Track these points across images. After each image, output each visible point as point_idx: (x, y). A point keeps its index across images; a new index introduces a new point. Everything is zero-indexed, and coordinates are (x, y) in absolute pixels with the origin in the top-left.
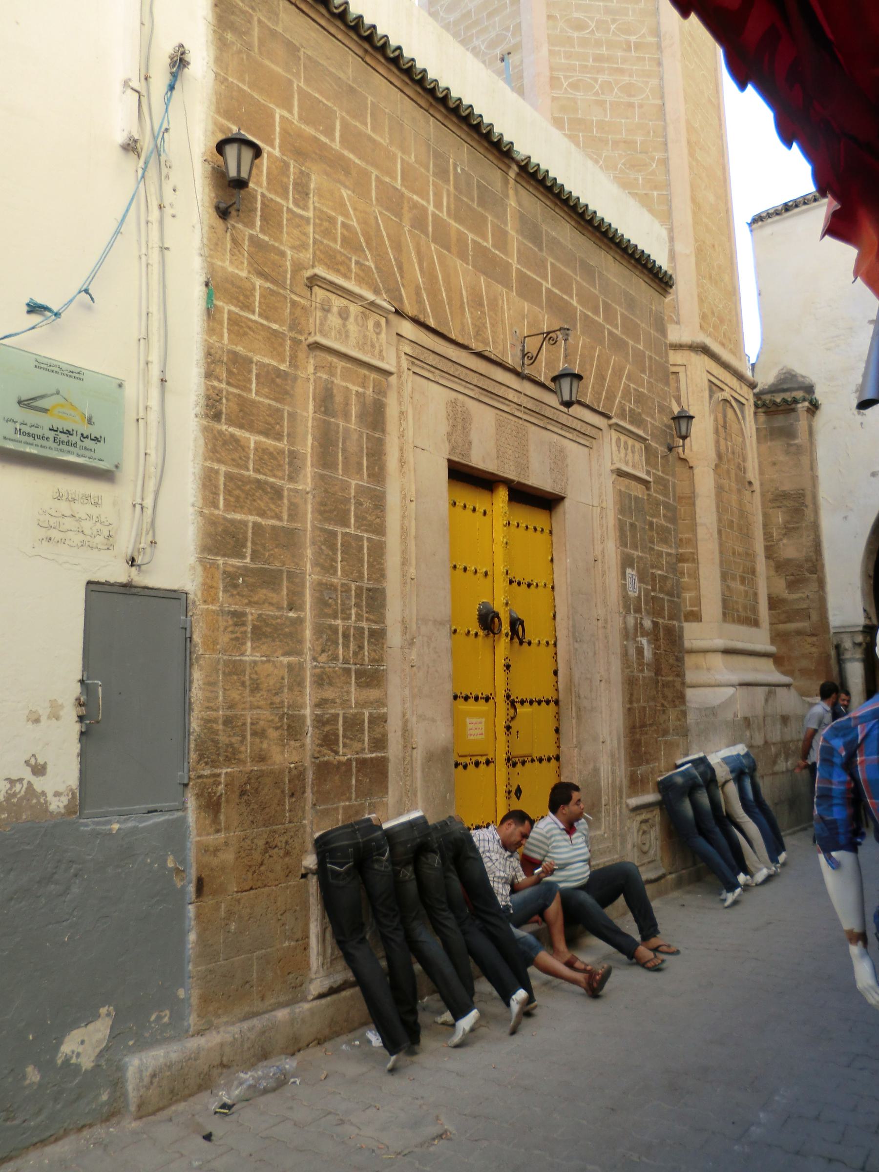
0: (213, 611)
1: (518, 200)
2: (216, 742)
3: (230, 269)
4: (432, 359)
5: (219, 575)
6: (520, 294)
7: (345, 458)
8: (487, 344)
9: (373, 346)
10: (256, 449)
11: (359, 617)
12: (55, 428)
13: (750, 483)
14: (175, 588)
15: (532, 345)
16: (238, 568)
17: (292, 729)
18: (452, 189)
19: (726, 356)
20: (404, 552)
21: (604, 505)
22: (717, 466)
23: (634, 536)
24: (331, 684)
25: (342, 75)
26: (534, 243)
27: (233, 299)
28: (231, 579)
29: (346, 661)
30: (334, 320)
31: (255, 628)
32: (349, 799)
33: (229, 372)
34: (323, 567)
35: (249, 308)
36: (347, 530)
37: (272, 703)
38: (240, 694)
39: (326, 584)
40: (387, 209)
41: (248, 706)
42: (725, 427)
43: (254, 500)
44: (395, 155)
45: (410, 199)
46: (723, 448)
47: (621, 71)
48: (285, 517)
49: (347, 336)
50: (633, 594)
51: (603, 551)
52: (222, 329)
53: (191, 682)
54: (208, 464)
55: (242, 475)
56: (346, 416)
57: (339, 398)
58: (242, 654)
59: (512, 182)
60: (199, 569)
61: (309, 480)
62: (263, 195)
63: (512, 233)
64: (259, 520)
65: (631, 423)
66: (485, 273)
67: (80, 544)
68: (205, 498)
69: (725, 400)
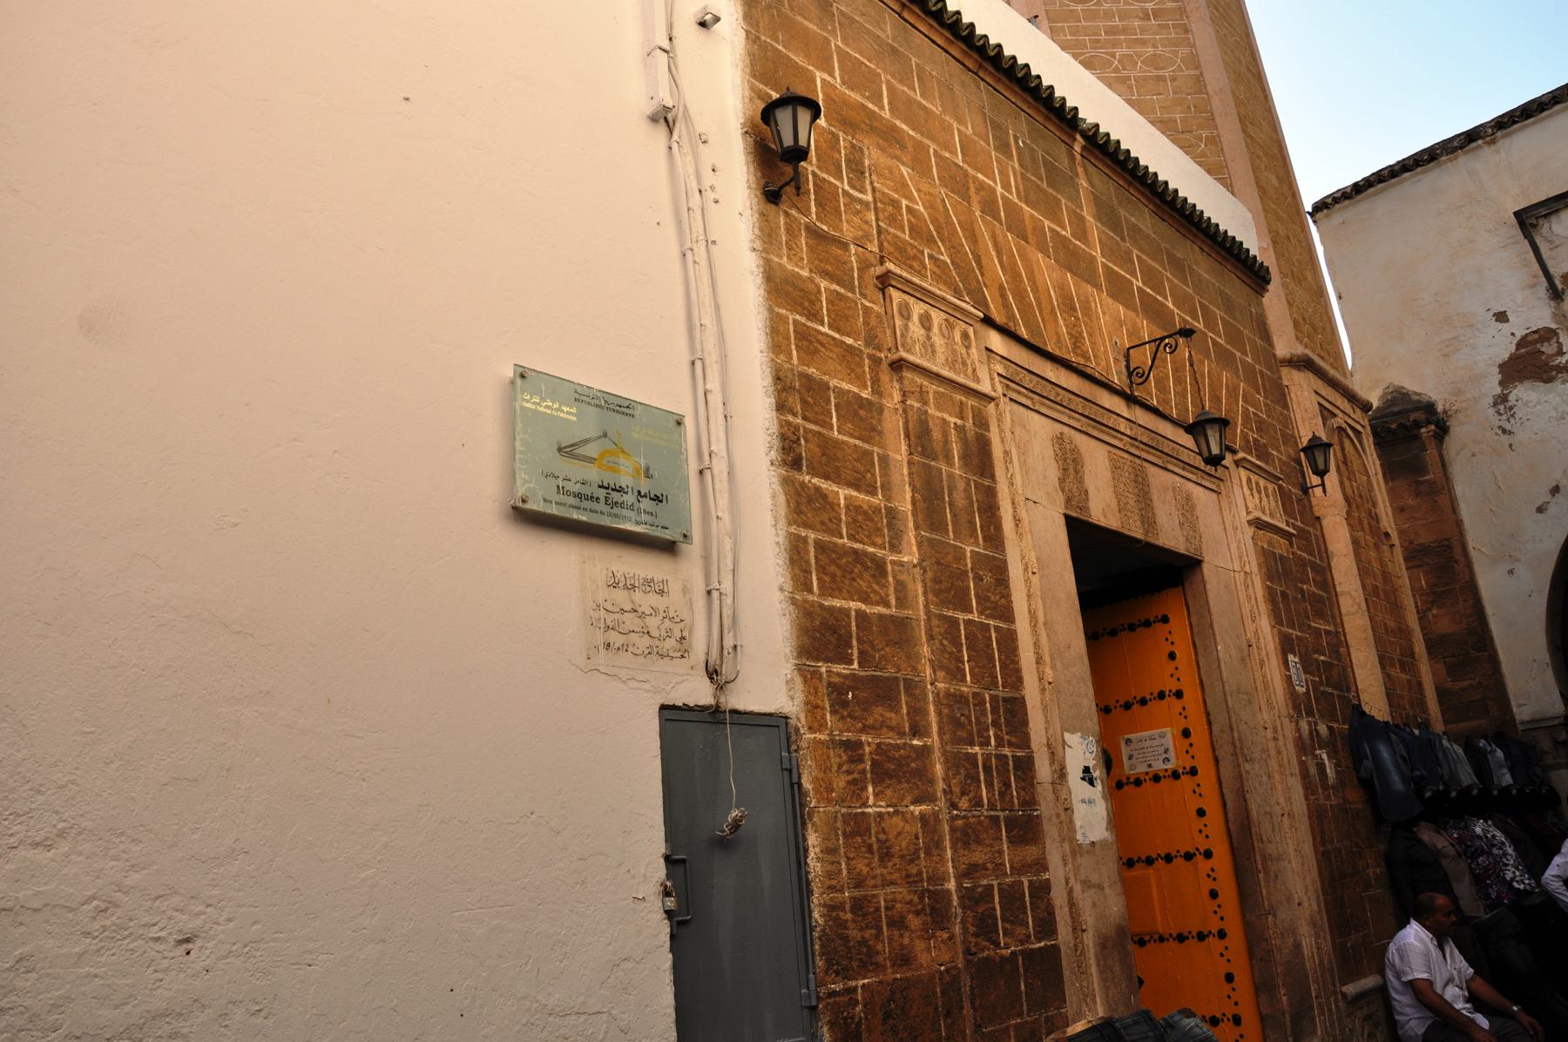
0: (821, 742)
1: (1088, 181)
2: (846, 939)
3: (790, 267)
4: (1029, 381)
5: (823, 690)
6: (1112, 296)
7: (954, 516)
9: (964, 363)
10: (847, 507)
11: (1000, 744)
13: (1387, 534)
14: (771, 709)
15: (1143, 357)
16: (845, 677)
17: (936, 911)
18: (1017, 165)
19: (1332, 372)
20: (1036, 645)
21: (1247, 569)
22: (1348, 513)
23: (1288, 611)
24: (978, 842)
25: (880, 33)
26: (1115, 231)
27: (796, 306)
28: (837, 691)
29: (992, 807)
30: (916, 330)
31: (874, 762)
32: (1020, 1014)
33: (804, 402)
34: (948, 671)
35: (815, 316)
36: (970, 617)
37: (908, 876)
38: (868, 865)
39: (954, 695)
41: (879, 882)
42: (1345, 463)
44: (950, 125)
45: (975, 179)
46: (1348, 490)
47: (1143, 43)
48: (893, 602)
49: (934, 352)
50: (1301, 690)
51: (1256, 633)
52: (789, 344)
53: (806, 850)
54: (793, 529)
55: (835, 544)
56: (948, 459)
57: (936, 434)
58: (865, 805)
59: (1078, 157)
60: (798, 680)
61: (915, 548)
62: (814, 174)
63: (1089, 218)
64: (863, 607)
65: (1259, 458)
66: (1071, 271)
68: (794, 578)
69: (1340, 428)
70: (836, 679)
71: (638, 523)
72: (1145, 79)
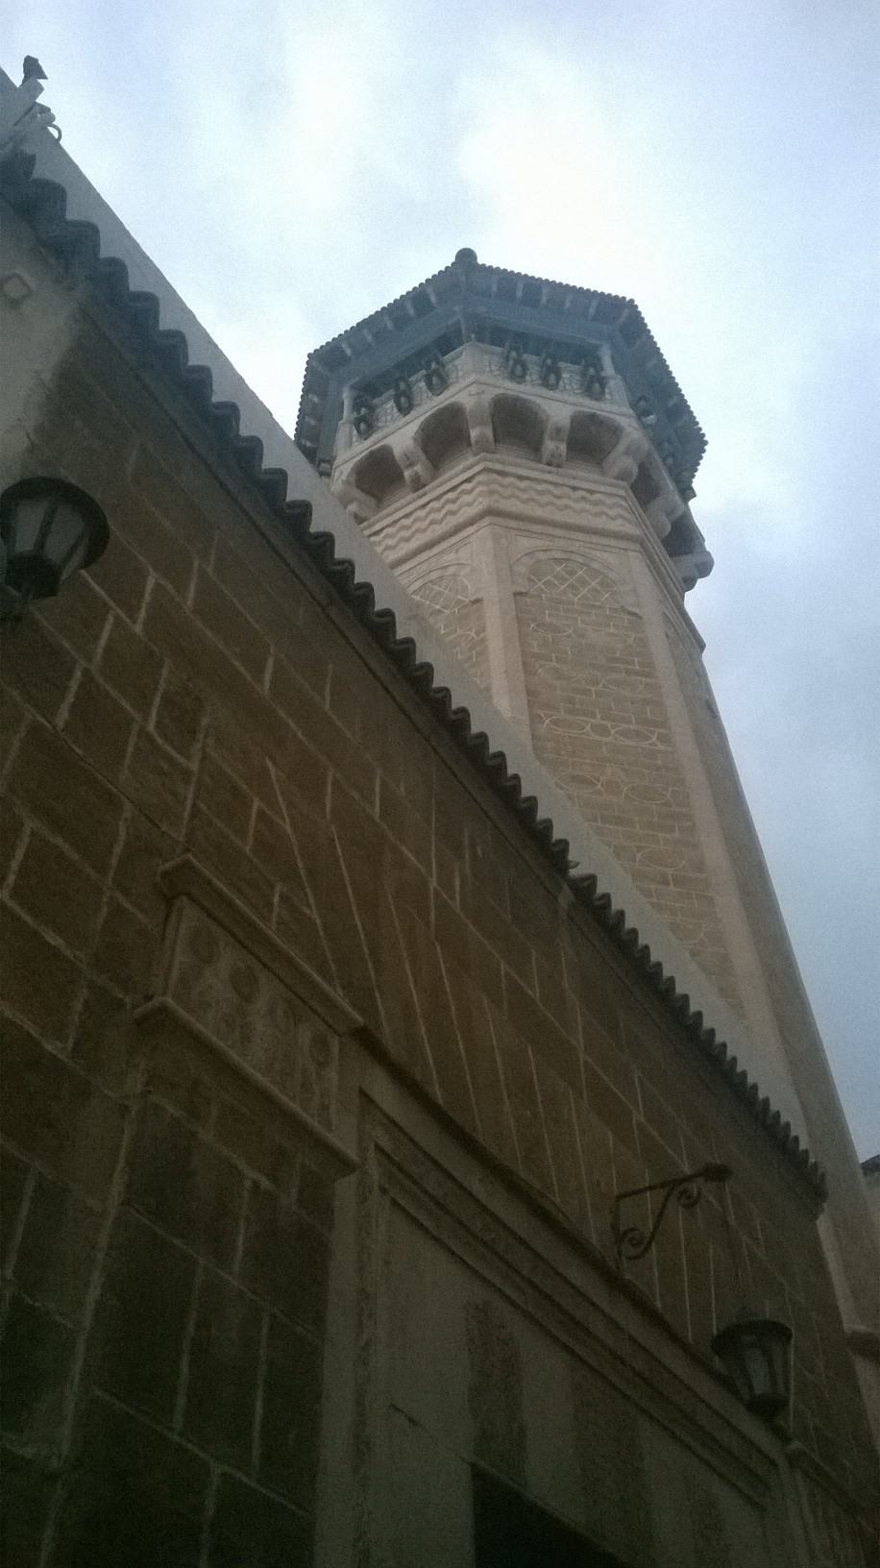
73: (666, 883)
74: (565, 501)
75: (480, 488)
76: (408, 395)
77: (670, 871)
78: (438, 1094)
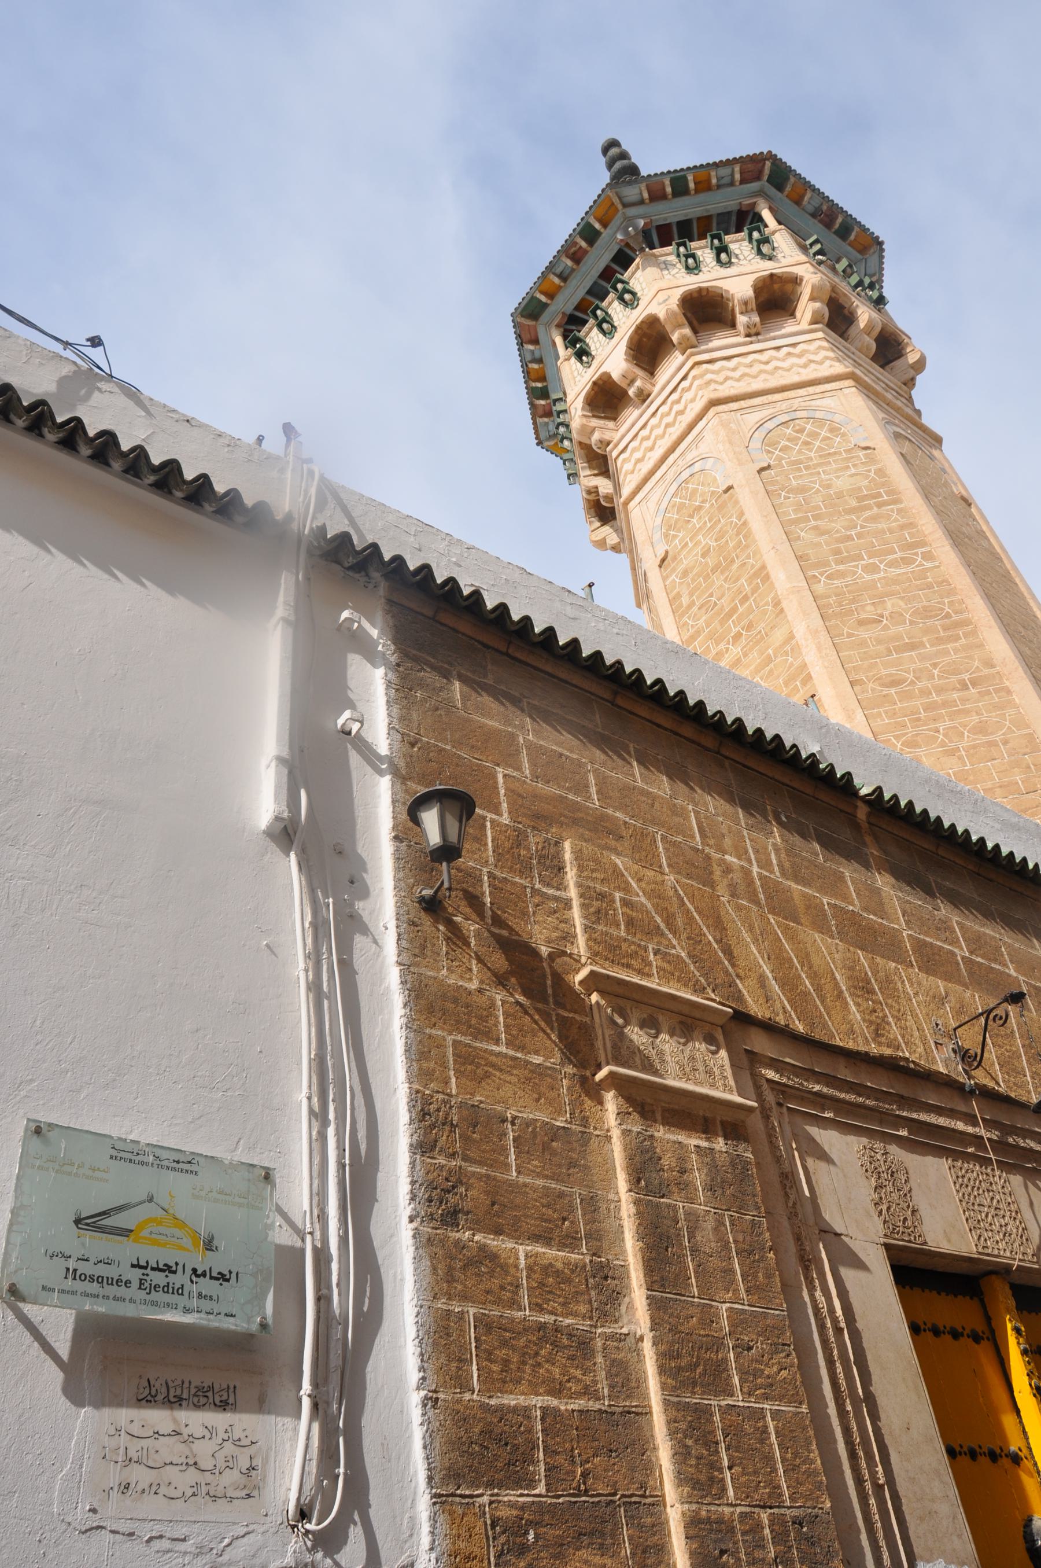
8: (898, 1047)
10: (530, 1269)
12: (143, 1263)
15: (969, 1038)
16: (523, 1507)
39: (708, 1521)
40: (689, 876)
43: (539, 1365)
47: (966, 712)
56: (685, 1187)
64: (554, 1402)
66: (862, 949)
67: (189, 1492)
70: (504, 1513)
71: (187, 1310)
72: (974, 747)
73: (964, 687)
74: (774, 364)
75: (697, 383)
76: (607, 319)
77: (966, 676)
78: (800, 1027)
